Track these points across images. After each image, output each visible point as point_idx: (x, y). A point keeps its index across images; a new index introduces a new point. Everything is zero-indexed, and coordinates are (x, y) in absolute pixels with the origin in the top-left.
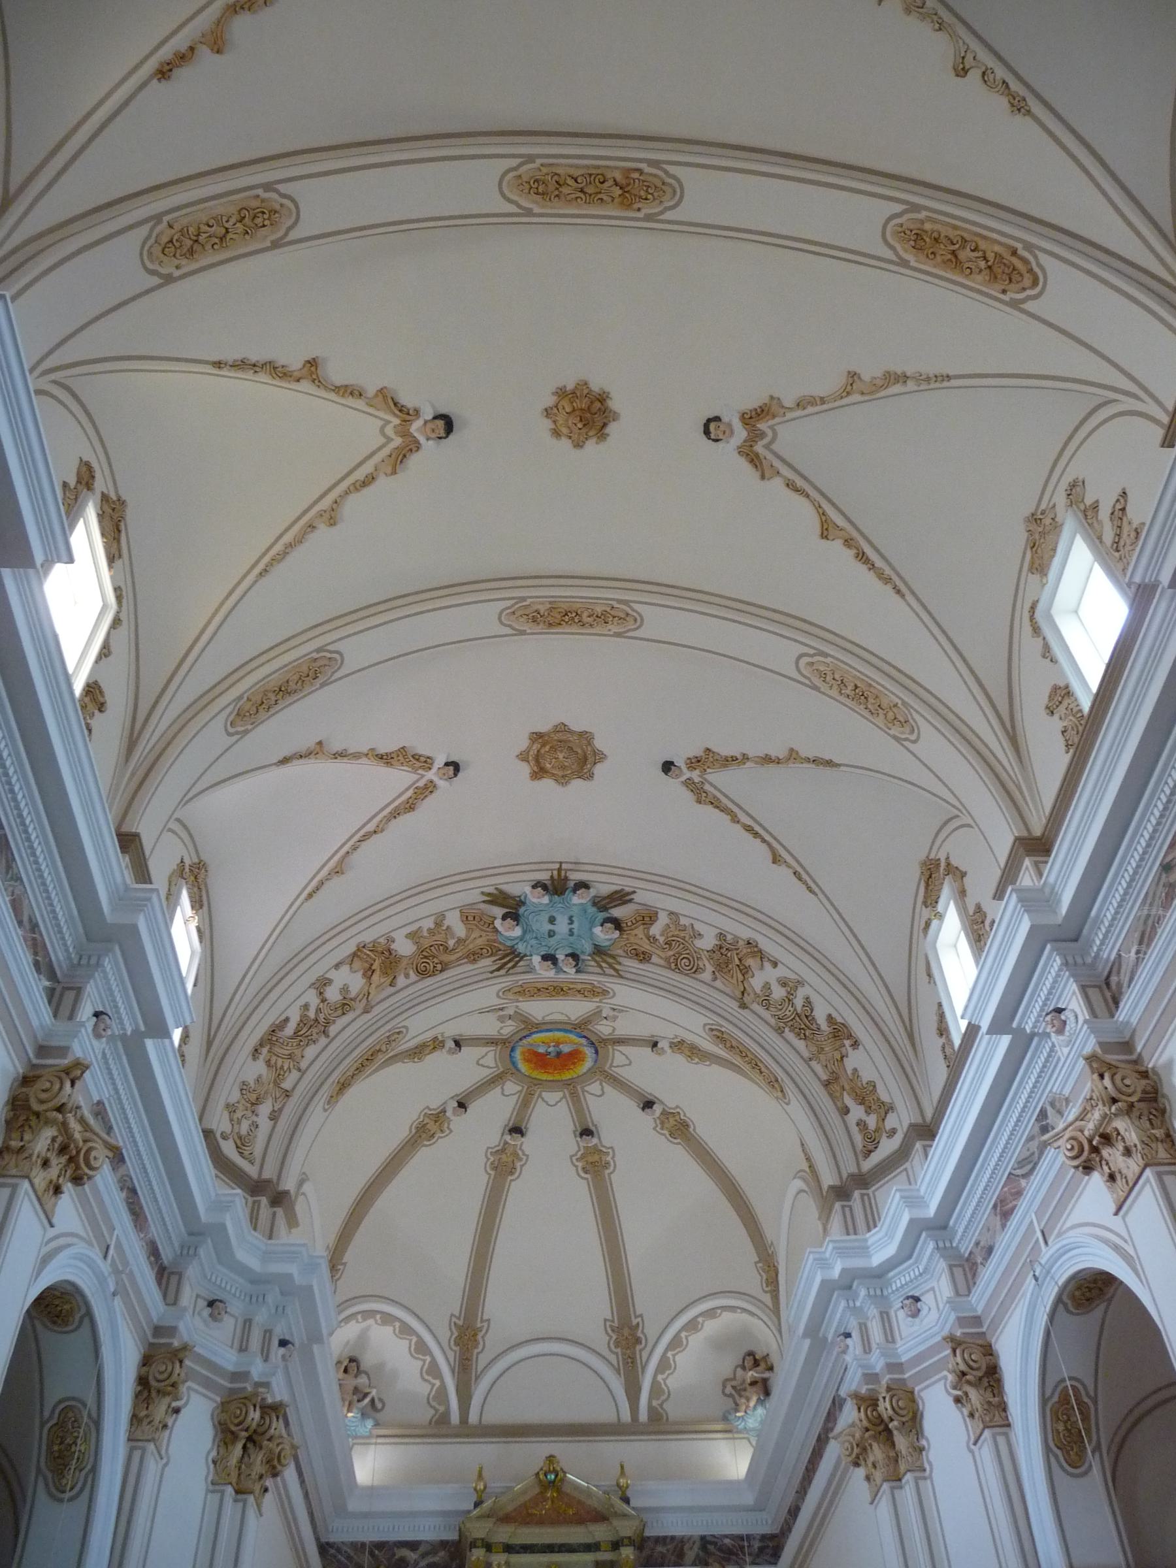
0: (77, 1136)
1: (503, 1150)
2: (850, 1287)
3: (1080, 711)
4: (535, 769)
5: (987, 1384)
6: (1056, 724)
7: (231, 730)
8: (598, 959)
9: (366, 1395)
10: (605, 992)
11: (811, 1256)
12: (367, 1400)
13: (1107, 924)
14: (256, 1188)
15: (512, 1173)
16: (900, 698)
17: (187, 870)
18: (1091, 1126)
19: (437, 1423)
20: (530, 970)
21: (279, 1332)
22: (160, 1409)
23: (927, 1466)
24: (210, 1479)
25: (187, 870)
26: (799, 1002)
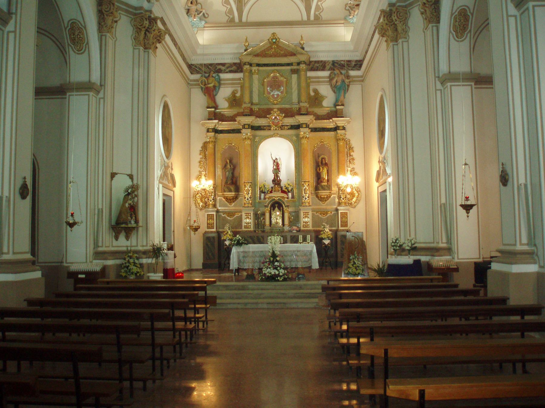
5: (433, 8)
9: (201, 12)
12: (201, 14)
24: (134, 44)
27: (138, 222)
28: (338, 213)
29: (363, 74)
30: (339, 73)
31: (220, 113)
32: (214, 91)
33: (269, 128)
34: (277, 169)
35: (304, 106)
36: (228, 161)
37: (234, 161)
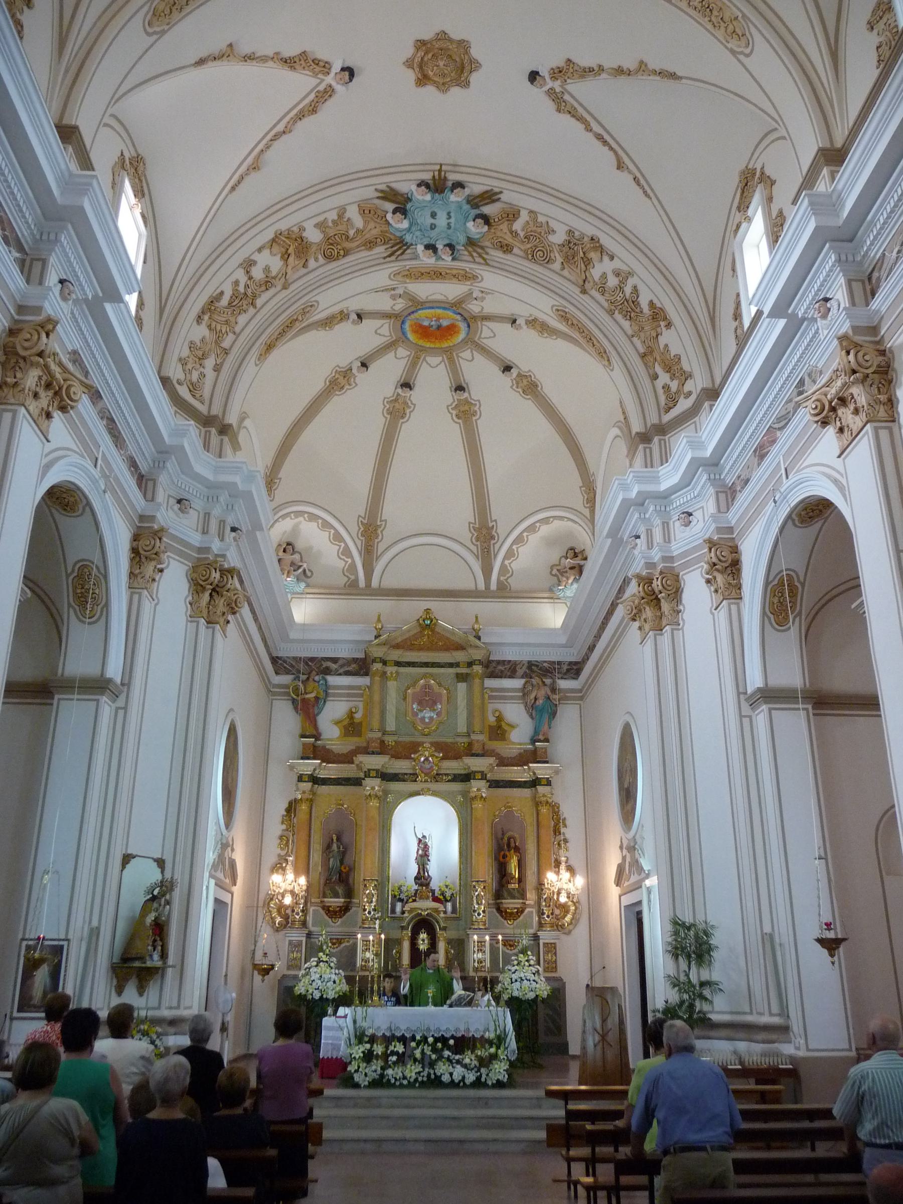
0: (58, 376)
1: (396, 400)
2: (643, 504)
3: (897, 26)
4: (419, 76)
6: (874, 39)
7: (150, 30)
8: (470, 249)
9: (300, 567)
10: (475, 277)
11: (617, 482)
12: (301, 570)
13: (878, 227)
14: (206, 421)
15: (403, 417)
16: (741, 11)
17: (127, 162)
18: (833, 391)
19: (350, 586)
20: (416, 257)
21: (231, 521)
22: (149, 569)
23: (681, 622)
24: (189, 613)
25: (127, 162)
26: (628, 290)
27: (167, 958)
28: (539, 944)
29: (583, 687)
30: (540, 683)
31: (324, 747)
32: (316, 708)
33: (413, 777)
34: (423, 857)
35: (478, 741)
36: (335, 838)
37: (345, 839)
